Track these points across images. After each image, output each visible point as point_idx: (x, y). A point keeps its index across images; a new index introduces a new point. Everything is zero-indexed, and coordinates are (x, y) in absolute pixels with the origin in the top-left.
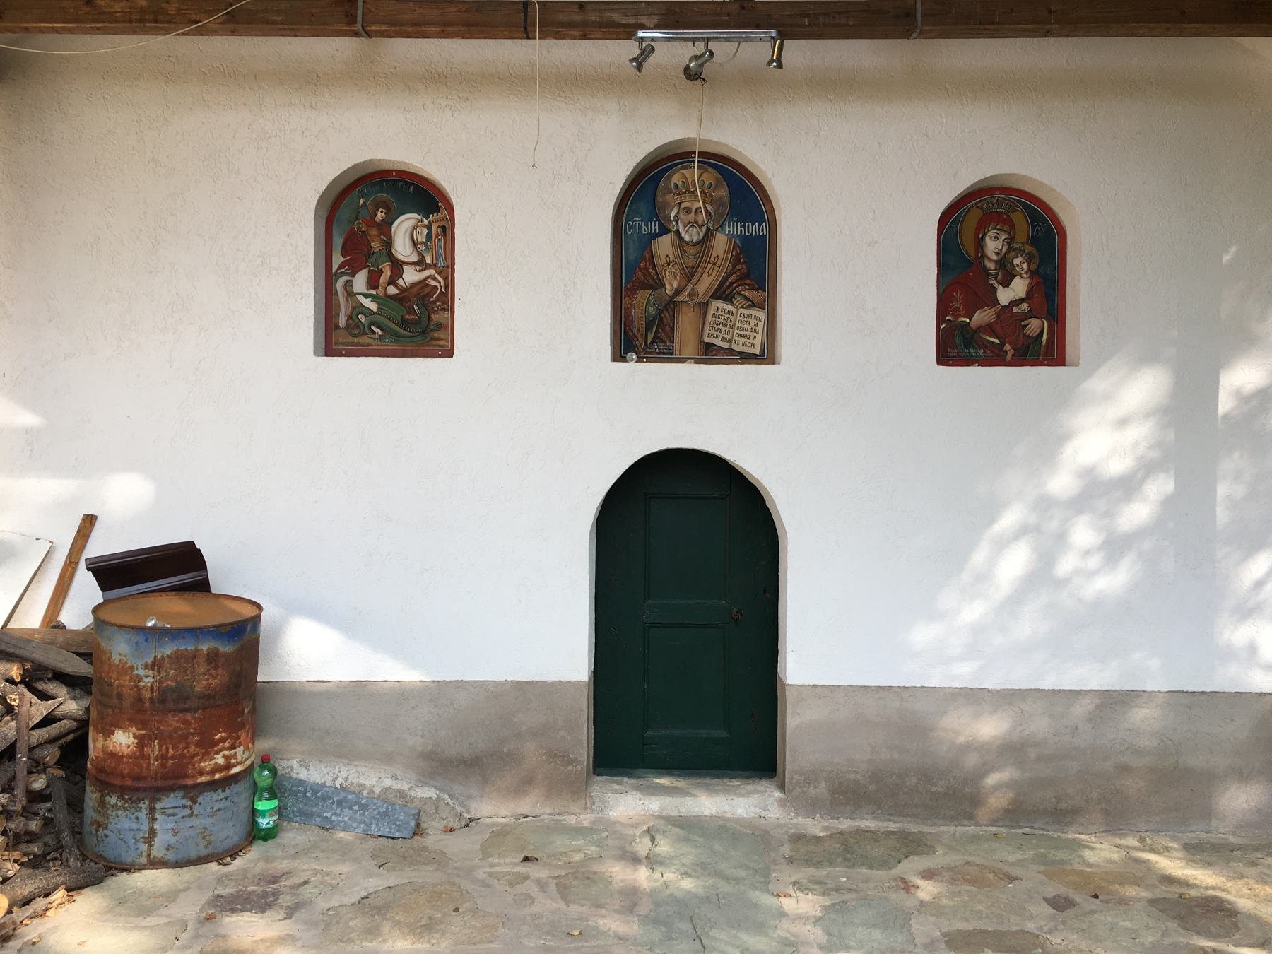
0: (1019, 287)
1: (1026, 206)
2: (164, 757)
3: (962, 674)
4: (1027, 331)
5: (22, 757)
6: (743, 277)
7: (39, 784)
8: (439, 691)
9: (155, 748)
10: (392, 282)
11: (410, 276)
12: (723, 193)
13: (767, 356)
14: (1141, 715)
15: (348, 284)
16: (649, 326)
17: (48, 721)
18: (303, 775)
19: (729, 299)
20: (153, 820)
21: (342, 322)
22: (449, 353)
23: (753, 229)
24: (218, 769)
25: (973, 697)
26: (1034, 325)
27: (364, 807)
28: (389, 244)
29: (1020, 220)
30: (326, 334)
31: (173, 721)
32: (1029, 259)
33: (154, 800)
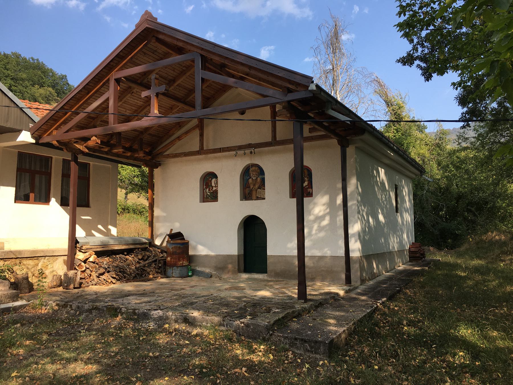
1: (307, 169)
2: (174, 261)
4: (308, 191)
5: (158, 261)
7: (160, 265)
8: (217, 256)
10: (212, 190)
12: (259, 171)
17: (162, 257)
18: (198, 269)
19: (260, 189)
20: (173, 270)
24: (181, 264)
28: (211, 184)
30: (16, 175)
31: (174, 256)
32: (308, 178)
33: (173, 268)
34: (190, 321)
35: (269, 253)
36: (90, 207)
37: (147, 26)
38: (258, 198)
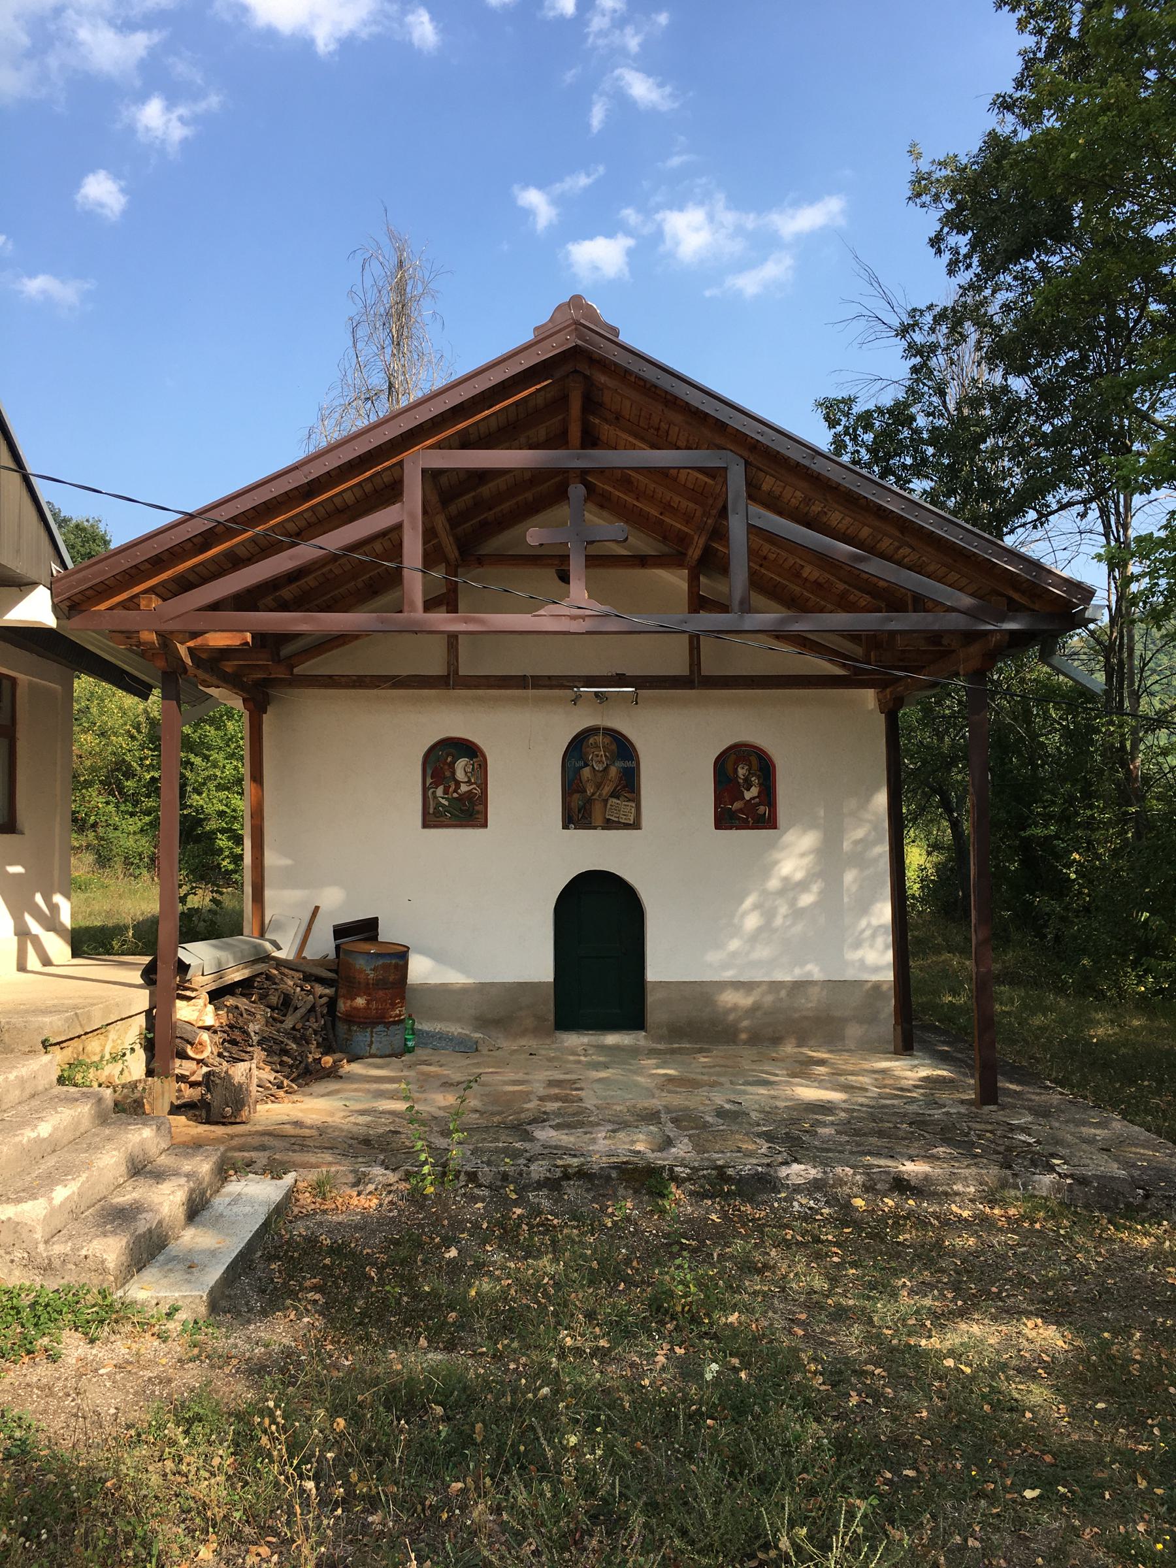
0: (754, 791)
3: (728, 975)
6: (624, 787)
9: (374, 1005)
10: (455, 791)
11: (464, 788)
12: (614, 747)
13: (636, 825)
14: (814, 992)
15: (434, 793)
16: (579, 811)
21: (431, 811)
22: (485, 825)
23: (629, 764)
25: (737, 985)
26: (762, 809)
27: (451, 1040)
28: (454, 773)
29: (754, 761)
34: (913, 1184)
35: (652, 975)
36: (22, 833)
37: (580, 342)
38: (609, 825)
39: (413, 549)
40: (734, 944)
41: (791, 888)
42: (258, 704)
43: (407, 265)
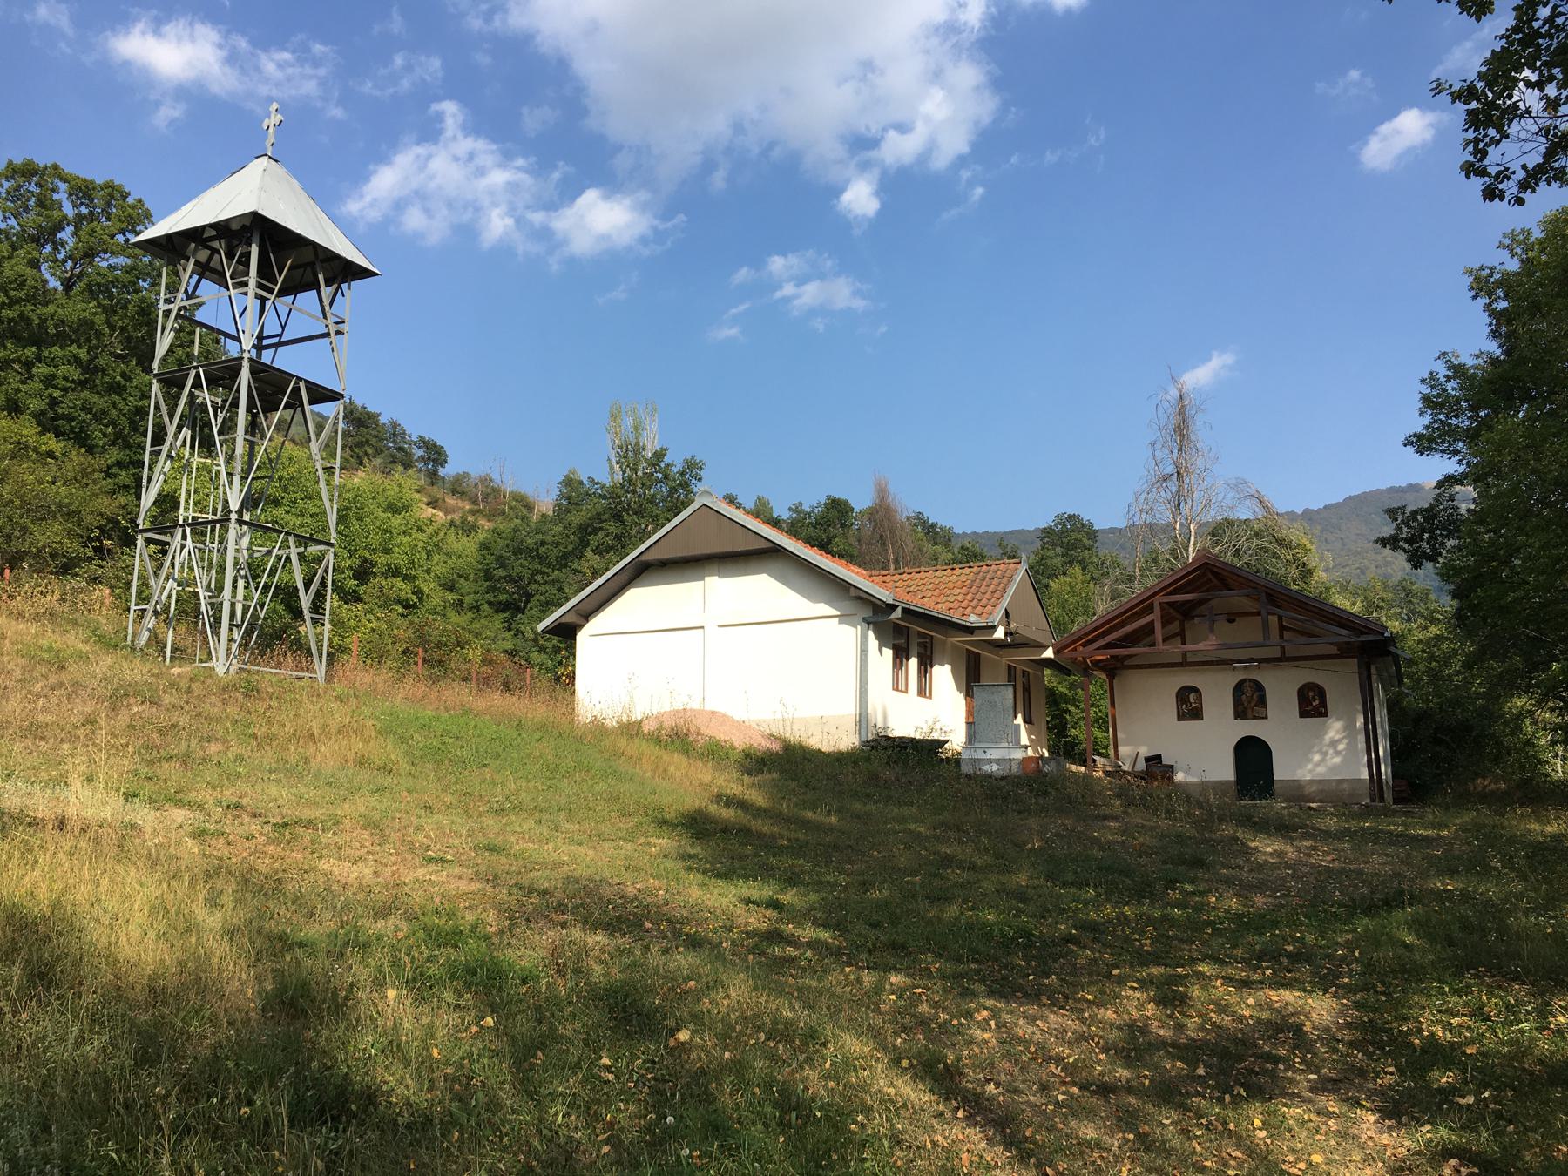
0: (1317, 702)
11: (1194, 705)
13: (1266, 717)
39: (1158, 626)
40: (1310, 766)
41: (1334, 743)
42: (1111, 677)
43: (1185, 396)
